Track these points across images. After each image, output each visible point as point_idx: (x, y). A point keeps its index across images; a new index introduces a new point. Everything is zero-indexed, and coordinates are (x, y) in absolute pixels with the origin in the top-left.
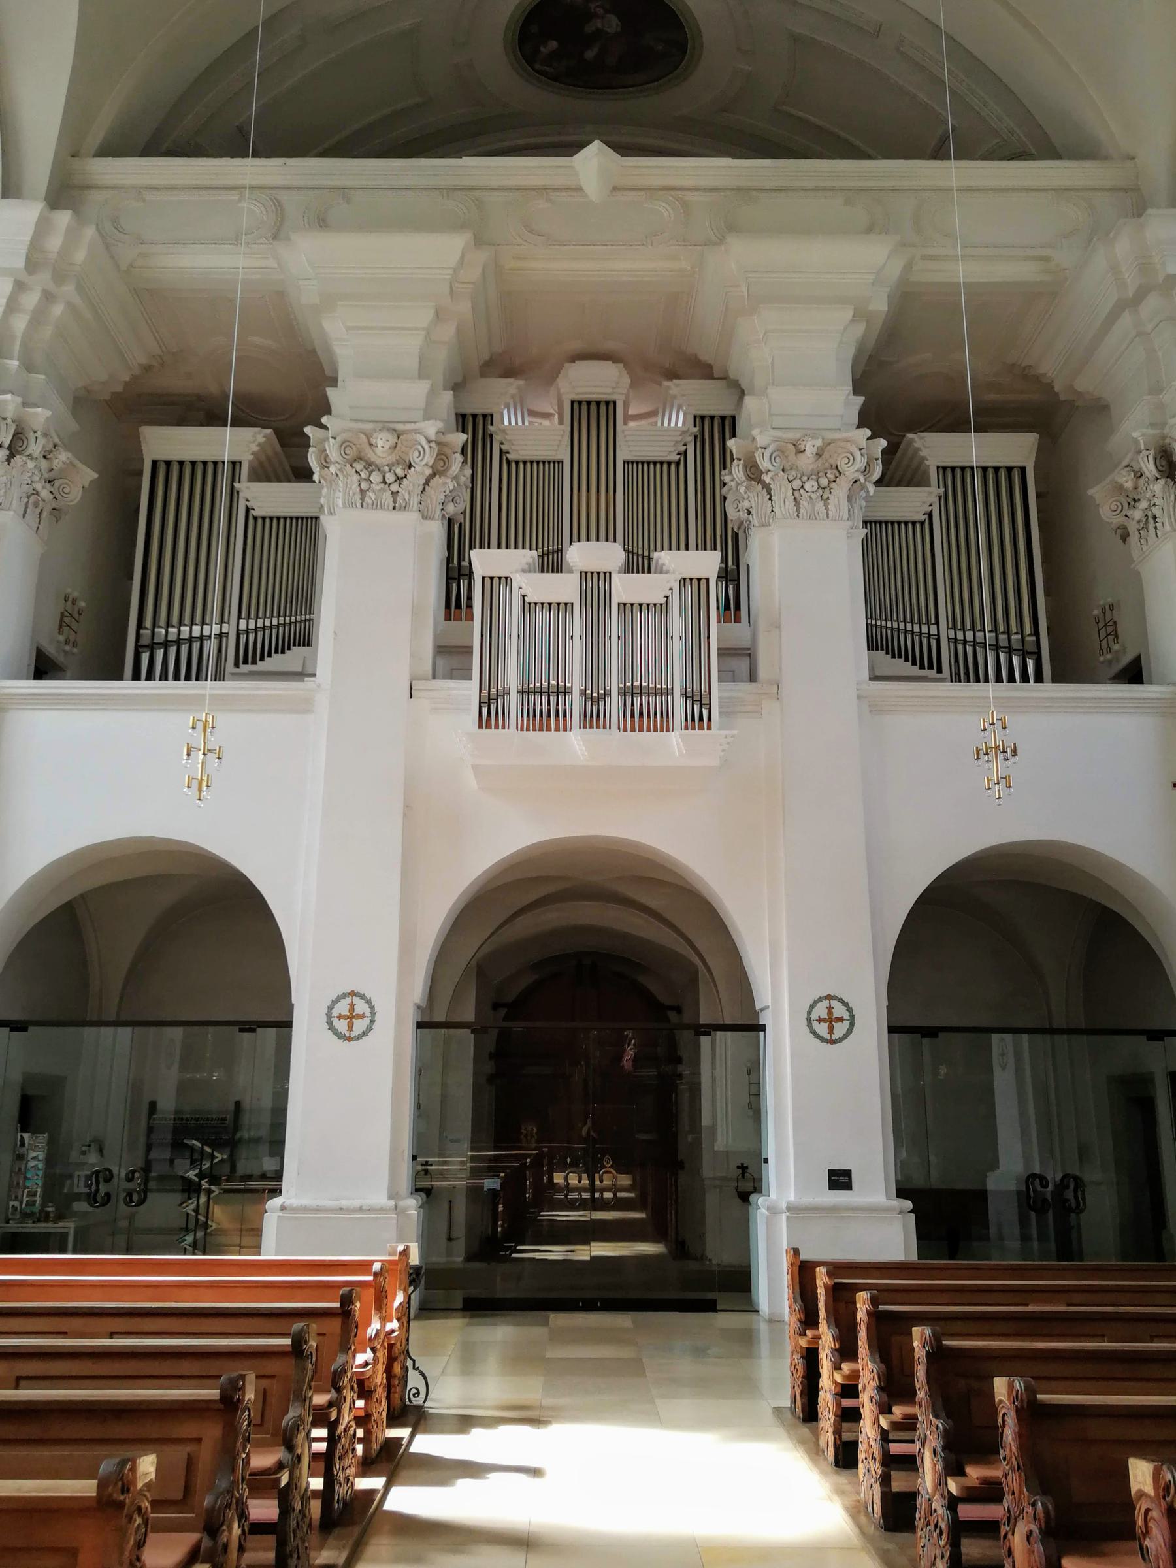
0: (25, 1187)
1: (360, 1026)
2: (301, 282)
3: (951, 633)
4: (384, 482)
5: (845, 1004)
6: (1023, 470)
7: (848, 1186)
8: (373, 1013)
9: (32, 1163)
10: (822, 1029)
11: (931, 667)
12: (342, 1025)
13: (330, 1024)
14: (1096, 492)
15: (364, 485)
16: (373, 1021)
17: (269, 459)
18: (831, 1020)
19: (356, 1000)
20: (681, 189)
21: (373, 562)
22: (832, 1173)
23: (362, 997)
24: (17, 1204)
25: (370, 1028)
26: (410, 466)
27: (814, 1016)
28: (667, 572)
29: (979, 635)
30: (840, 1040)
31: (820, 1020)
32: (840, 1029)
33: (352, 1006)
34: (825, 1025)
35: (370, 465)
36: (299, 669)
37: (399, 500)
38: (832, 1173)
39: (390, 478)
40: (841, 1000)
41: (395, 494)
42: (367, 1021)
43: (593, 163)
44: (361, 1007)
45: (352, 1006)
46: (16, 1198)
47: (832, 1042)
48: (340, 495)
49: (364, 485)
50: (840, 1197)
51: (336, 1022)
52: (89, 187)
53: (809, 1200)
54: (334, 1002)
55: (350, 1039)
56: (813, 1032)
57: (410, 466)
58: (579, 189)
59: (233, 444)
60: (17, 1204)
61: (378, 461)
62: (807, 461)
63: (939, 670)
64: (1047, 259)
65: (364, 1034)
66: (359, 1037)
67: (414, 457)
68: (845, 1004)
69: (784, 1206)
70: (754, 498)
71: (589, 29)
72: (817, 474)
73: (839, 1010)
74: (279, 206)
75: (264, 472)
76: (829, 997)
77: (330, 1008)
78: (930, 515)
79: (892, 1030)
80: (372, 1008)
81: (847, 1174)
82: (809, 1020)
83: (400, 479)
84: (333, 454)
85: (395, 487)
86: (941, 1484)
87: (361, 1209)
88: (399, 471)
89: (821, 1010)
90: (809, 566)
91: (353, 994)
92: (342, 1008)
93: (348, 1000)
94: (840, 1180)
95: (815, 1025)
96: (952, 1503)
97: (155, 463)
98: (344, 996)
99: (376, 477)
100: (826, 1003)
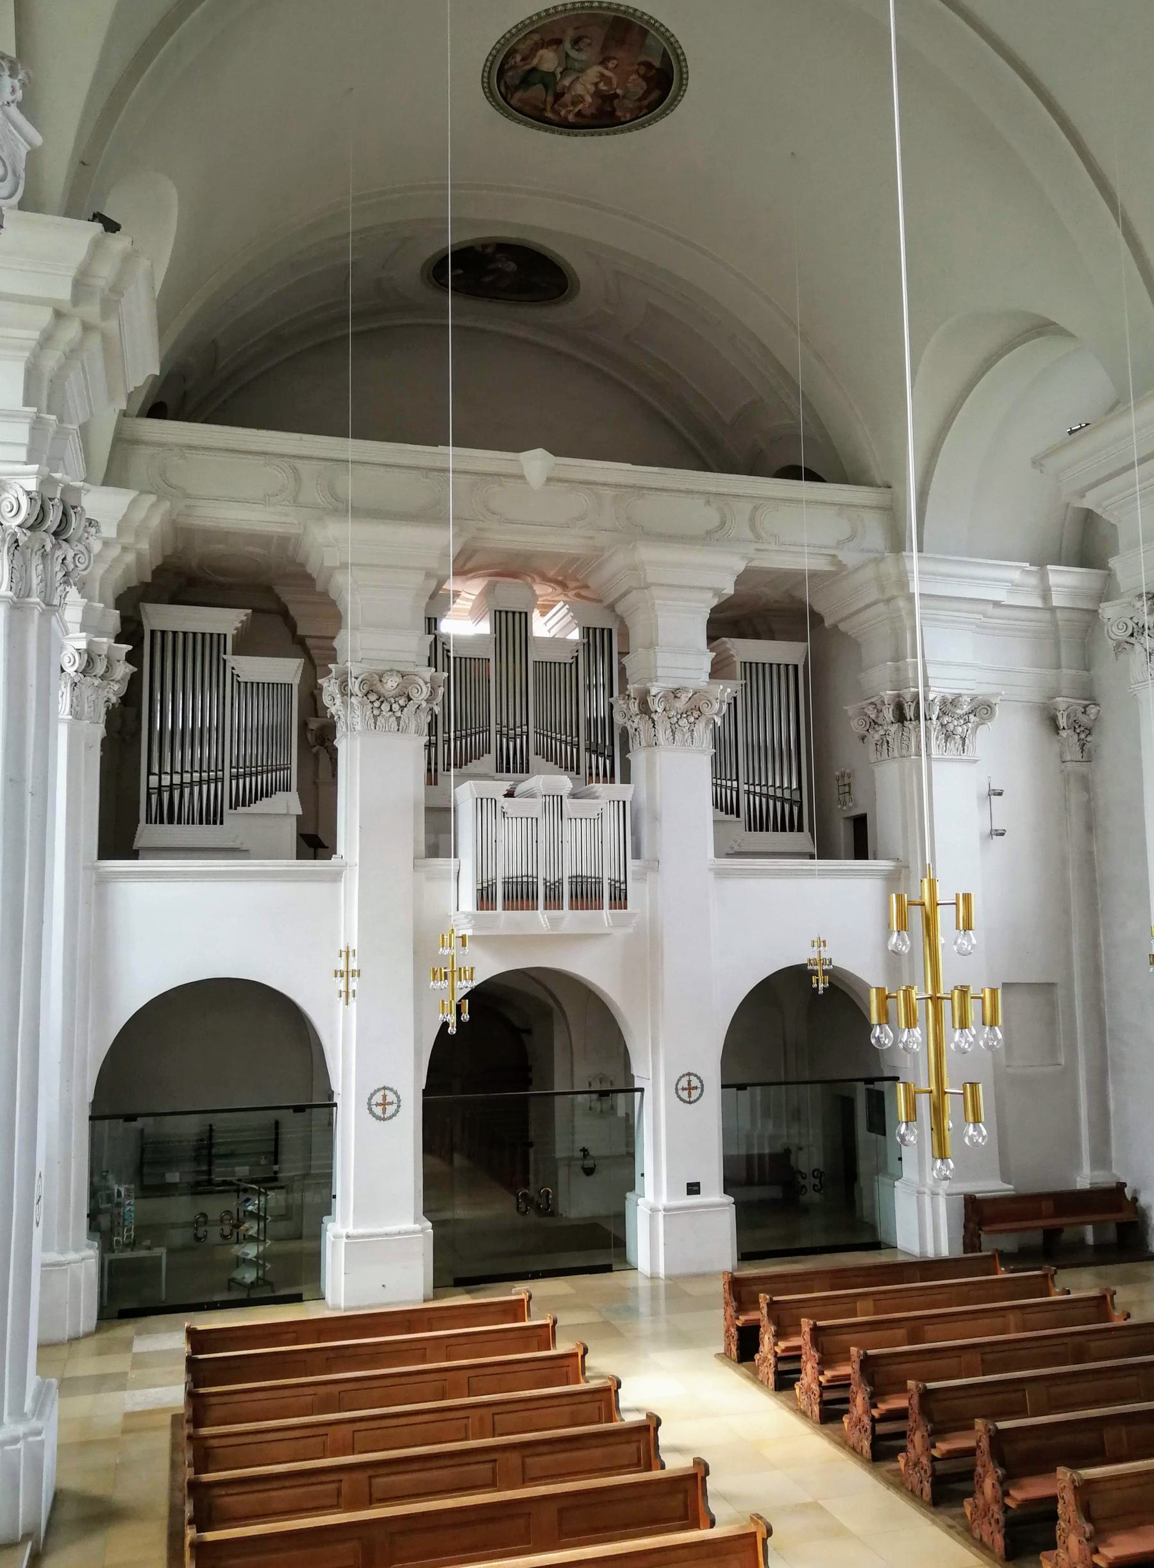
0: (124, 1226)
1: (390, 1110)
2: (324, 549)
3: (746, 787)
4: (391, 710)
5: (699, 1078)
6: (796, 667)
7: (698, 1192)
8: (399, 1101)
9: (128, 1208)
10: (684, 1095)
11: (732, 813)
12: (378, 1110)
13: (370, 1109)
14: (850, 709)
15: (376, 712)
16: (399, 1106)
17: (761, 1156)
18: (690, 1089)
19: (387, 1092)
20: (596, 484)
21: (377, 769)
22: (689, 1185)
23: (391, 1090)
24: (120, 1239)
25: (397, 1111)
26: (410, 699)
27: (680, 1087)
28: (597, 798)
29: (764, 788)
30: (695, 1101)
31: (683, 1089)
32: (695, 1094)
33: (385, 1097)
34: (686, 1092)
35: (382, 699)
36: (285, 812)
37: (402, 723)
38: (689, 1185)
39: (396, 707)
40: (696, 1076)
41: (398, 719)
42: (395, 1106)
43: (536, 463)
44: (391, 1097)
45: (385, 1097)
46: (118, 1235)
47: (690, 1103)
48: (359, 720)
49: (376, 712)
50: (694, 1200)
51: (374, 1108)
52: (137, 442)
53: (675, 1203)
54: (372, 1095)
55: (384, 1119)
56: (679, 1096)
57: (410, 699)
58: (522, 477)
59: (226, 621)
60: (120, 1239)
61: (386, 694)
62: (681, 704)
63: (738, 816)
64: (834, 556)
65: (394, 1115)
66: (390, 1118)
67: (414, 694)
68: (699, 1078)
69: (661, 1208)
70: (638, 723)
71: (491, 266)
72: (686, 713)
73: (695, 1082)
74: (297, 478)
75: (246, 644)
76: (689, 1074)
77: (370, 1099)
78: (735, 699)
79: (723, 1087)
80: (398, 1097)
81: (698, 1184)
82: (677, 1089)
83: (402, 708)
84: (354, 686)
85: (399, 714)
86: (867, 1412)
87: (399, 1233)
88: (402, 702)
89: (684, 1083)
90: (678, 776)
91: (384, 1088)
92: (378, 1098)
93: (382, 1092)
94: (693, 1189)
95: (680, 1092)
96: (874, 1420)
97: (153, 632)
98: (379, 1090)
99: (385, 707)
100: (687, 1078)
